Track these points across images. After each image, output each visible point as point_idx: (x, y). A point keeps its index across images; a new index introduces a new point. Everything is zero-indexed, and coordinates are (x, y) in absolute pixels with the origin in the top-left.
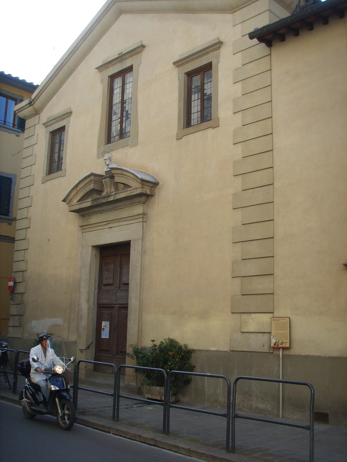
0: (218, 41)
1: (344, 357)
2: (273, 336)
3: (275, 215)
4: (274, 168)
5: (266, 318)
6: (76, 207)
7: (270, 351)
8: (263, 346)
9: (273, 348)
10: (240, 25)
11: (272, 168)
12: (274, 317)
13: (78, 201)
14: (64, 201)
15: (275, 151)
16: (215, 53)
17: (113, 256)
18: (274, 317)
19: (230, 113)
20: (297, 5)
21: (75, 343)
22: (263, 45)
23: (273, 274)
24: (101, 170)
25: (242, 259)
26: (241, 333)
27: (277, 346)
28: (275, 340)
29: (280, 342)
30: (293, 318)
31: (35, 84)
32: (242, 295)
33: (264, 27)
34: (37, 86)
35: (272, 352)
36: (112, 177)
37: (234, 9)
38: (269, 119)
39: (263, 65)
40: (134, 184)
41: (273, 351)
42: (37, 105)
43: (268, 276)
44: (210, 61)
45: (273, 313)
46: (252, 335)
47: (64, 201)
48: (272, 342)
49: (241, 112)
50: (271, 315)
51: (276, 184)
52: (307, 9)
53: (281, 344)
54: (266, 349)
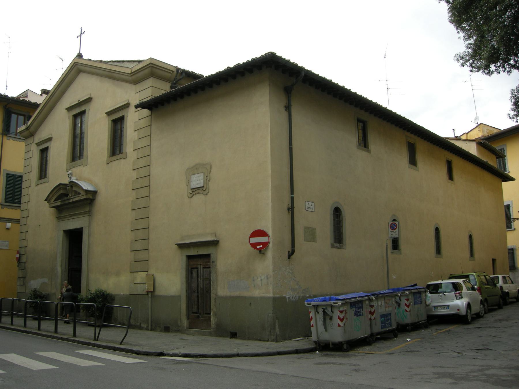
5: (144, 274)
6: (53, 205)
13: (55, 201)
14: (46, 200)
15: (151, 176)
17: (75, 239)
19: (132, 150)
21: (55, 294)
24: (66, 181)
31: (39, 103)
34: (39, 105)
36: (72, 186)
40: (83, 193)
42: (32, 129)
46: (139, 285)
47: (46, 200)
50: (147, 273)
51: (151, 196)
54: (144, 293)
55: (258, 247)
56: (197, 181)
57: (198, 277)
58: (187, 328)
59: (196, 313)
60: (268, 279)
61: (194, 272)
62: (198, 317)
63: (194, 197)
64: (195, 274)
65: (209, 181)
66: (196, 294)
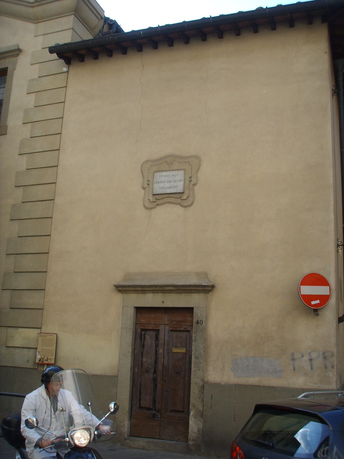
0: (17, 48)
1: (107, 375)
2: (39, 352)
3: (52, 231)
4: (57, 184)
5: (33, 333)
7: (34, 367)
8: (28, 361)
9: (38, 364)
10: (42, 37)
11: (55, 184)
12: (41, 333)
15: (60, 168)
16: (12, 59)
18: (42, 332)
19: (20, 123)
20: (100, 30)
22: (62, 61)
23: (45, 290)
25: (15, 272)
26: (5, 348)
27: (42, 362)
28: (41, 355)
29: (46, 358)
30: (61, 335)
32: (11, 308)
33: (65, 44)
35: (37, 368)
37: (38, 19)
38: (58, 135)
39: (59, 81)
41: (38, 368)
43: (40, 291)
44: (6, 66)
45: (40, 328)
48: (37, 358)
49: (31, 123)
50: (38, 331)
51: (58, 200)
52: (109, 36)
53: (46, 360)
54: (30, 365)
55: (313, 303)
56: (170, 181)
57: (157, 346)
58: (128, 436)
59: (149, 409)
60: (325, 358)
61: (148, 337)
62: (154, 416)
63: (158, 208)
64: (149, 339)
65: (195, 185)
66: (151, 376)
